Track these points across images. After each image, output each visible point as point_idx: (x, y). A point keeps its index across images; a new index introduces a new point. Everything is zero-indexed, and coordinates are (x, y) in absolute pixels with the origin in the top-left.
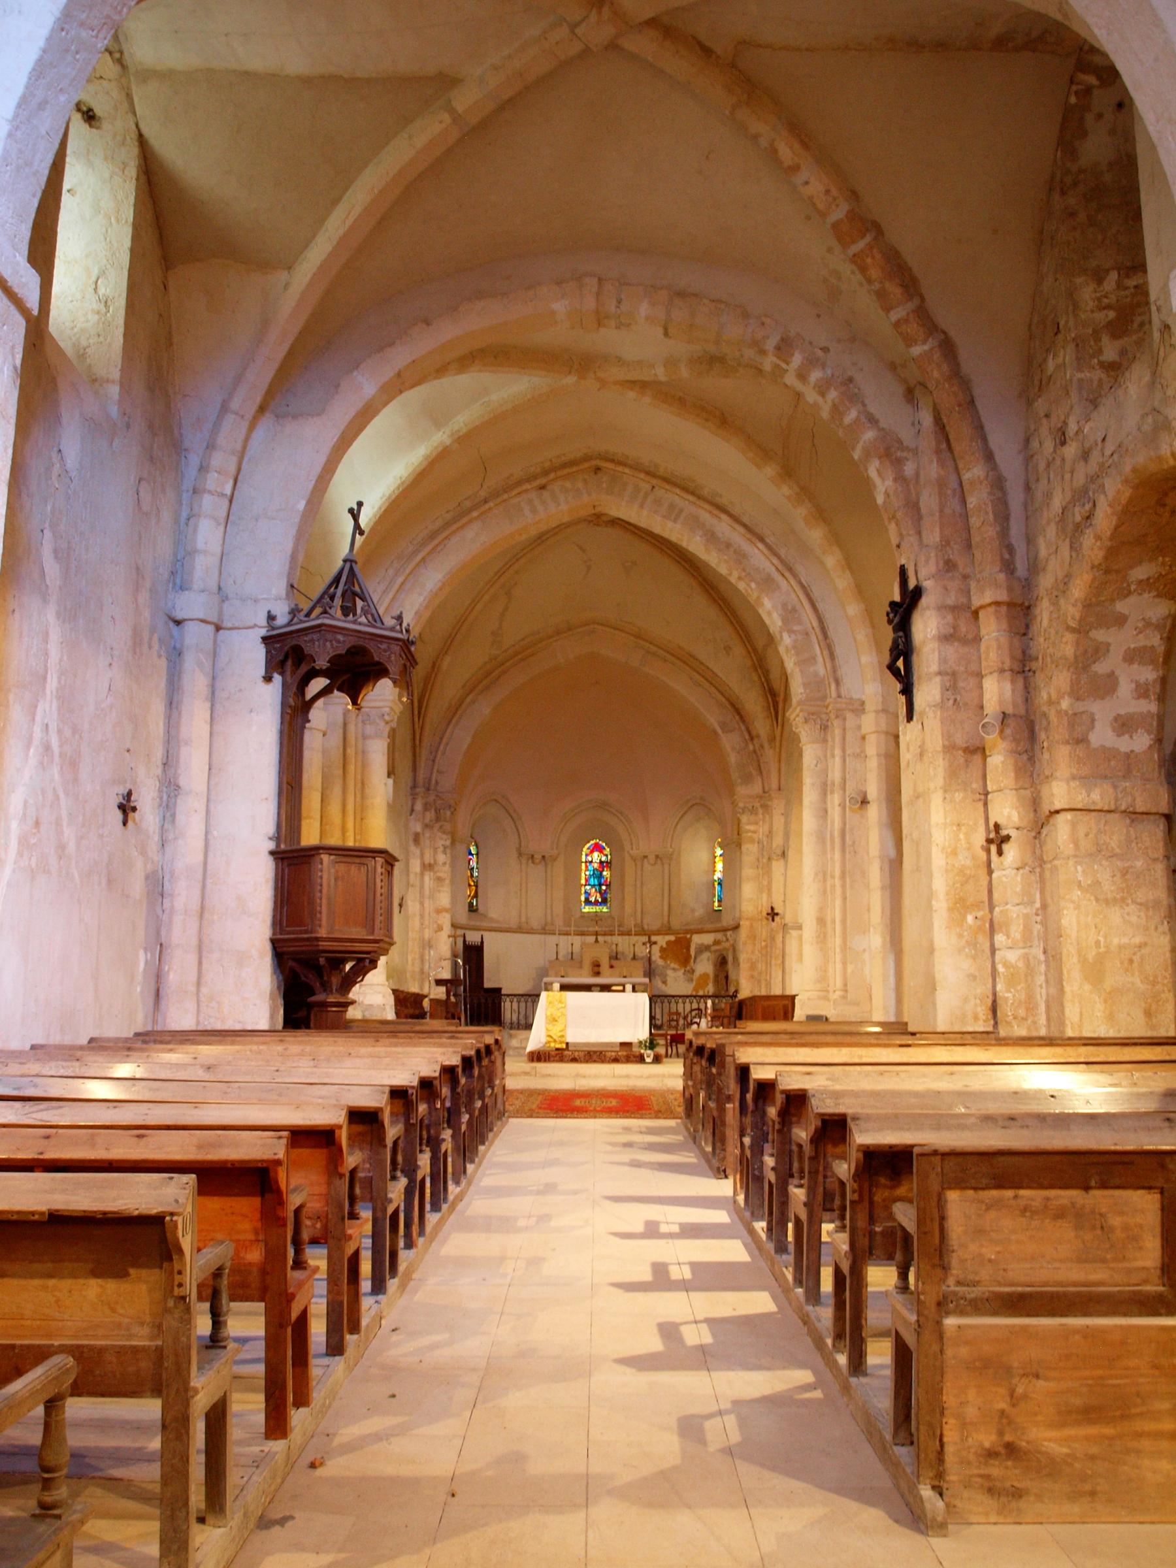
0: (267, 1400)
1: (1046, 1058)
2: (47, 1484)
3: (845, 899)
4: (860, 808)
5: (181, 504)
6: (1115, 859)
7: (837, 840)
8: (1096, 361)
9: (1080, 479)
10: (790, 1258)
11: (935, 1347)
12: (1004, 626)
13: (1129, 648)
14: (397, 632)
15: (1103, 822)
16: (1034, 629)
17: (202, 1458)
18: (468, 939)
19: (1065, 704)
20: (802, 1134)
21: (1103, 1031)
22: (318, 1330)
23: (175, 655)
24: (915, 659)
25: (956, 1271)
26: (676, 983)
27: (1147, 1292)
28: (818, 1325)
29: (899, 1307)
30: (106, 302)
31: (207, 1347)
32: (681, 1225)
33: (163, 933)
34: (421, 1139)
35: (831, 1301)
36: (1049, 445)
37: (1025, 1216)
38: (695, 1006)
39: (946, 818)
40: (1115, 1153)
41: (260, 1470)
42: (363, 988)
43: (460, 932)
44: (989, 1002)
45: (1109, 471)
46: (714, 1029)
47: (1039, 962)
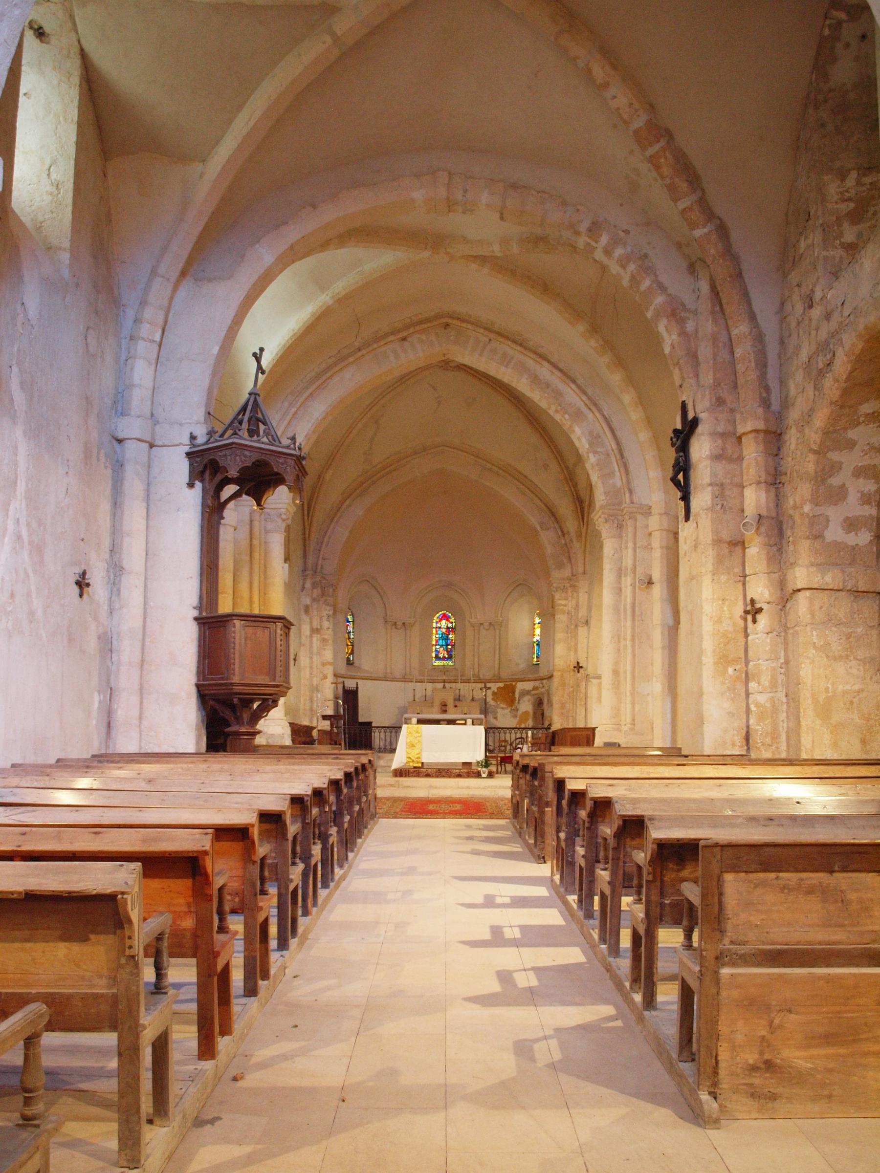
0: (199, 1031)
1: (789, 774)
2: (27, 1102)
3: (634, 656)
4: (647, 588)
5: (121, 348)
6: (841, 626)
7: (629, 612)
8: (838, 242)
9: (823, 334)
10: (596, 922)
11: (714, 990)
12: (761, 448)
13: (857, 466)
14: (290, 449)
15: (833, 599)
16: (784, 450)
17: (150, 1075)
18: (346, 685)
19: (807, 508)
20: (607, 830)
21: (830, 755)
22: (237, 977)
23: (118, 466)
24: (692, 474)
25: (730, 934)
26: (505, 718)
27: (875, 949)
28: (618, 972)
29: (685, 960)
30: (57, 186)
31: (152, 993)
32: (511, 897)
33: (112, 677)
34: (314, 834)
35: (629, 954)
36: (799, 308)
37: (783, 893)
38: (519, 735)
39: (713, 595)
40: (854, 845)
41: (194, 1083)
42: (267, 722)
43: (340, 680)
44: (744, 732)
45: (846, 328)
46: (534, 753)
47: (782, 702)
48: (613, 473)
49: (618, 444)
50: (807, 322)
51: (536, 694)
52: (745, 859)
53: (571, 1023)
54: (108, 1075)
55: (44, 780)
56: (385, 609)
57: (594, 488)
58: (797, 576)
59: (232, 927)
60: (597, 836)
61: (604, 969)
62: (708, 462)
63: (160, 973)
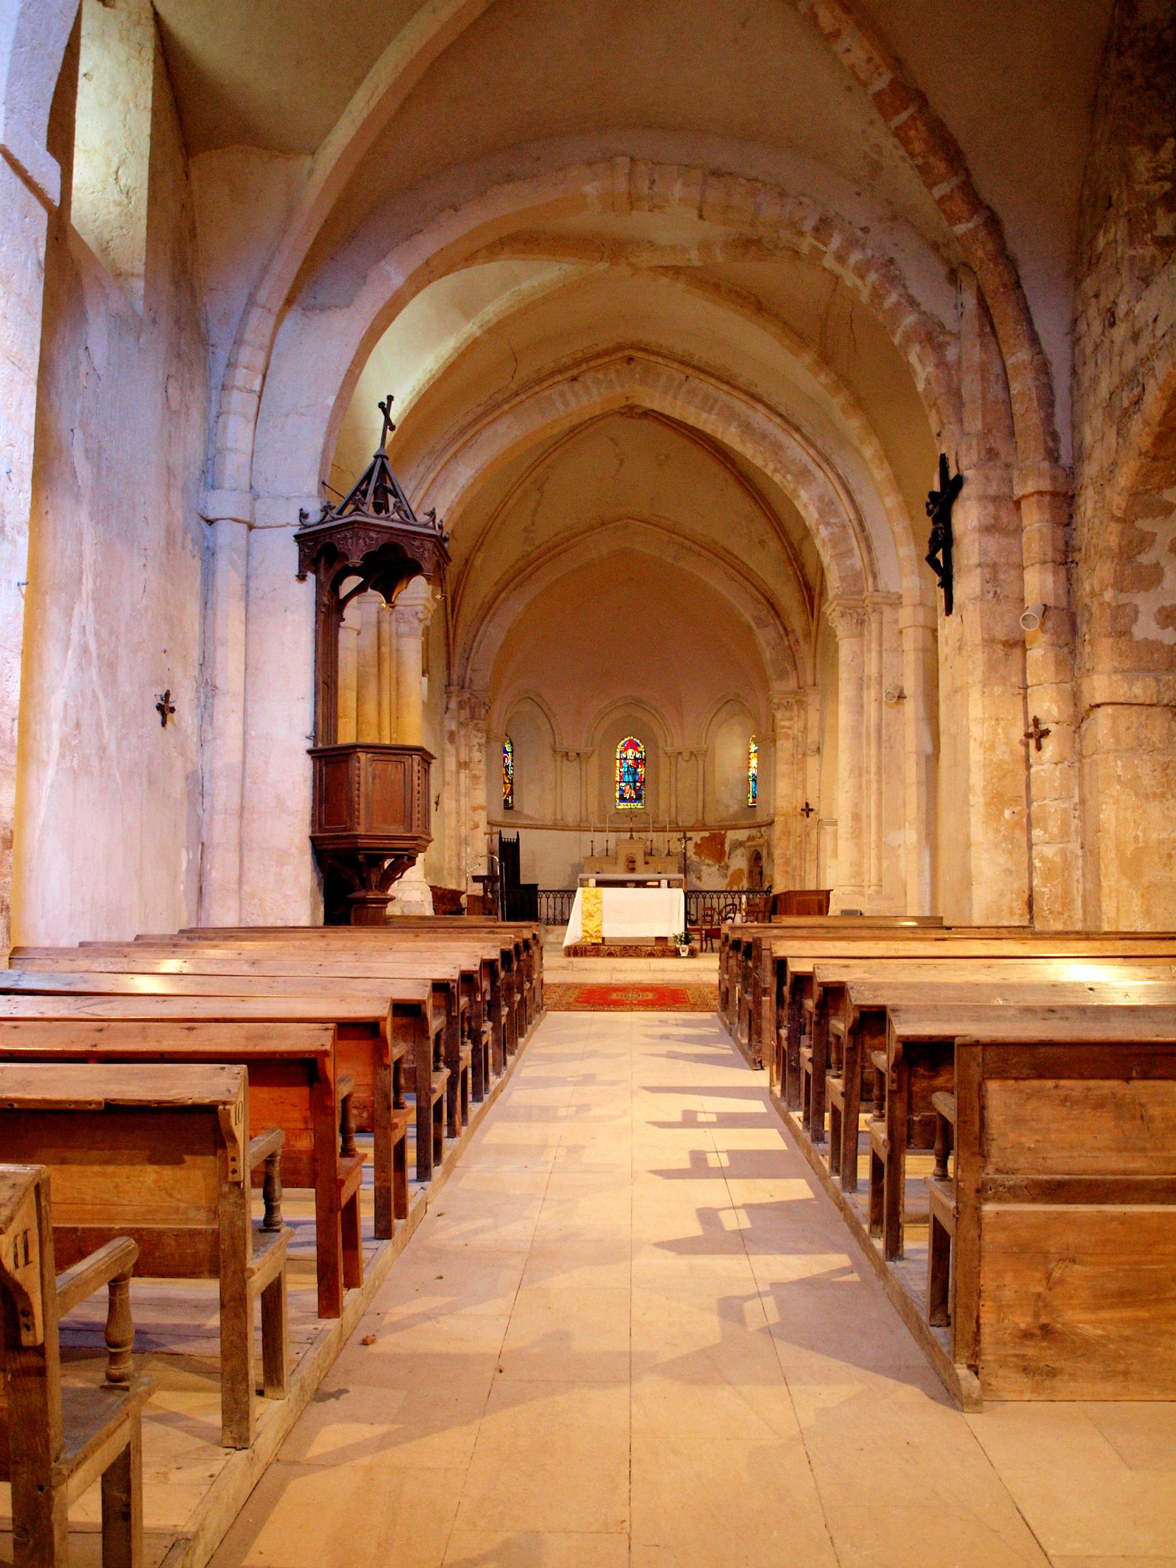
0: (319, 1281)
2: (114, 1359)
5: (210, 402)
6: (1155, 752)
7: (873, 736)
8: (1149, 236)
9: (1129, 362)
10: (827, 1147)
11: (974, 1233)
14: (430, 528)
15: (1143, 717)
16: (1078, 519)
17: (259, 1335)
19: (1108, 596)
20: (840, 1026)
21: (1140, 926)
22: (367, 1215)
23: (209, 554)
25: (996, 1157)
26: (711, 878)
28: (854, 1211)
29: (938, 1194)
30: (127, 193)
31: (261, 1231)
32: (717, 1114)
34: (463, 1031)
35: (868, 1188)
36: (1097, 327)
38: (729, 901)
39: (984, 713)
42: (402, 885)
43: (496, 829)
44: (1026, 896)
45: (1159, 352)
46: (749, 924)
47: (1076, 856)
48: (851, 551)
49: (857, 511)
50: (1107, 345)
51: (752, 846)
52: (1014, 1061)
53: (793, 1276)
54: (208, 1336)
55: (121, 963)
56: (554, 734)
57: (825, 571)
58: (1096, 686)
59: (360, 1151)
60: (828, 1032)
61: (836, 1207)
62: (976, 536)
63: (270, 1209)
